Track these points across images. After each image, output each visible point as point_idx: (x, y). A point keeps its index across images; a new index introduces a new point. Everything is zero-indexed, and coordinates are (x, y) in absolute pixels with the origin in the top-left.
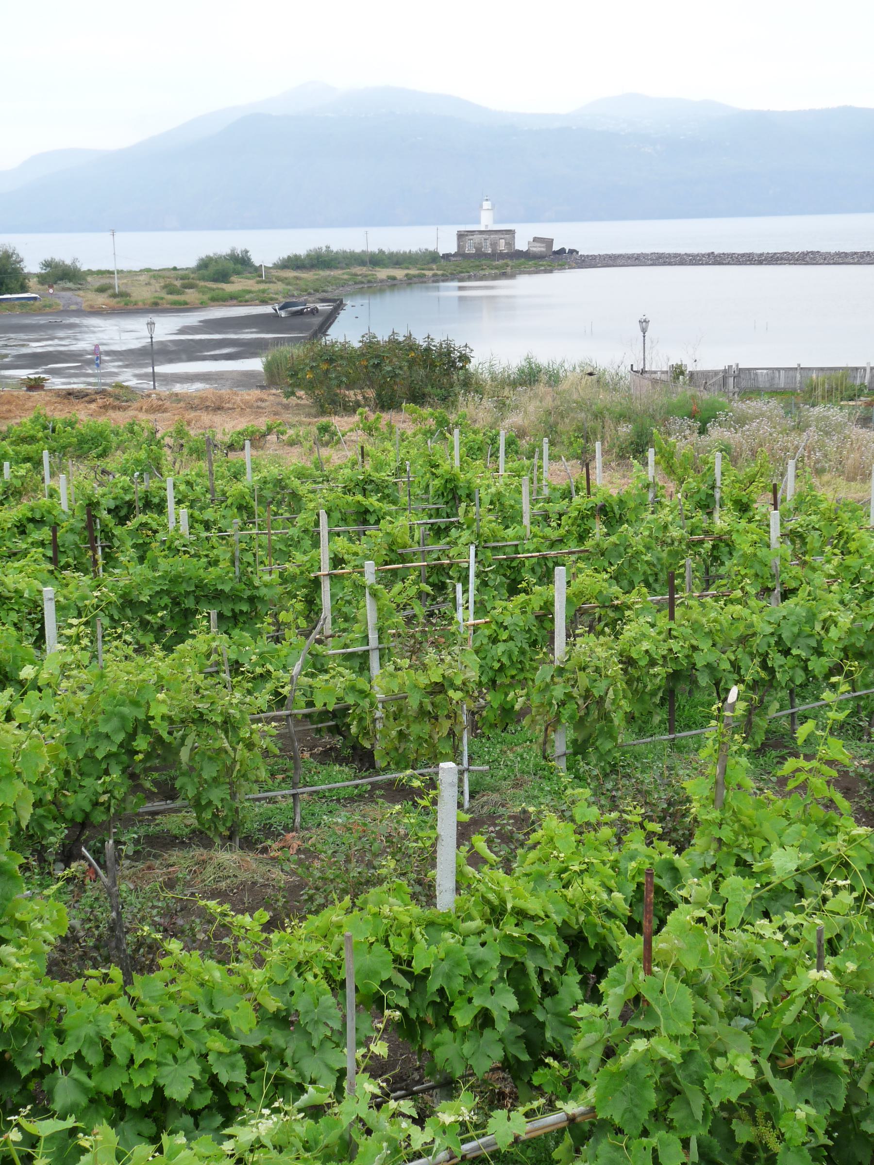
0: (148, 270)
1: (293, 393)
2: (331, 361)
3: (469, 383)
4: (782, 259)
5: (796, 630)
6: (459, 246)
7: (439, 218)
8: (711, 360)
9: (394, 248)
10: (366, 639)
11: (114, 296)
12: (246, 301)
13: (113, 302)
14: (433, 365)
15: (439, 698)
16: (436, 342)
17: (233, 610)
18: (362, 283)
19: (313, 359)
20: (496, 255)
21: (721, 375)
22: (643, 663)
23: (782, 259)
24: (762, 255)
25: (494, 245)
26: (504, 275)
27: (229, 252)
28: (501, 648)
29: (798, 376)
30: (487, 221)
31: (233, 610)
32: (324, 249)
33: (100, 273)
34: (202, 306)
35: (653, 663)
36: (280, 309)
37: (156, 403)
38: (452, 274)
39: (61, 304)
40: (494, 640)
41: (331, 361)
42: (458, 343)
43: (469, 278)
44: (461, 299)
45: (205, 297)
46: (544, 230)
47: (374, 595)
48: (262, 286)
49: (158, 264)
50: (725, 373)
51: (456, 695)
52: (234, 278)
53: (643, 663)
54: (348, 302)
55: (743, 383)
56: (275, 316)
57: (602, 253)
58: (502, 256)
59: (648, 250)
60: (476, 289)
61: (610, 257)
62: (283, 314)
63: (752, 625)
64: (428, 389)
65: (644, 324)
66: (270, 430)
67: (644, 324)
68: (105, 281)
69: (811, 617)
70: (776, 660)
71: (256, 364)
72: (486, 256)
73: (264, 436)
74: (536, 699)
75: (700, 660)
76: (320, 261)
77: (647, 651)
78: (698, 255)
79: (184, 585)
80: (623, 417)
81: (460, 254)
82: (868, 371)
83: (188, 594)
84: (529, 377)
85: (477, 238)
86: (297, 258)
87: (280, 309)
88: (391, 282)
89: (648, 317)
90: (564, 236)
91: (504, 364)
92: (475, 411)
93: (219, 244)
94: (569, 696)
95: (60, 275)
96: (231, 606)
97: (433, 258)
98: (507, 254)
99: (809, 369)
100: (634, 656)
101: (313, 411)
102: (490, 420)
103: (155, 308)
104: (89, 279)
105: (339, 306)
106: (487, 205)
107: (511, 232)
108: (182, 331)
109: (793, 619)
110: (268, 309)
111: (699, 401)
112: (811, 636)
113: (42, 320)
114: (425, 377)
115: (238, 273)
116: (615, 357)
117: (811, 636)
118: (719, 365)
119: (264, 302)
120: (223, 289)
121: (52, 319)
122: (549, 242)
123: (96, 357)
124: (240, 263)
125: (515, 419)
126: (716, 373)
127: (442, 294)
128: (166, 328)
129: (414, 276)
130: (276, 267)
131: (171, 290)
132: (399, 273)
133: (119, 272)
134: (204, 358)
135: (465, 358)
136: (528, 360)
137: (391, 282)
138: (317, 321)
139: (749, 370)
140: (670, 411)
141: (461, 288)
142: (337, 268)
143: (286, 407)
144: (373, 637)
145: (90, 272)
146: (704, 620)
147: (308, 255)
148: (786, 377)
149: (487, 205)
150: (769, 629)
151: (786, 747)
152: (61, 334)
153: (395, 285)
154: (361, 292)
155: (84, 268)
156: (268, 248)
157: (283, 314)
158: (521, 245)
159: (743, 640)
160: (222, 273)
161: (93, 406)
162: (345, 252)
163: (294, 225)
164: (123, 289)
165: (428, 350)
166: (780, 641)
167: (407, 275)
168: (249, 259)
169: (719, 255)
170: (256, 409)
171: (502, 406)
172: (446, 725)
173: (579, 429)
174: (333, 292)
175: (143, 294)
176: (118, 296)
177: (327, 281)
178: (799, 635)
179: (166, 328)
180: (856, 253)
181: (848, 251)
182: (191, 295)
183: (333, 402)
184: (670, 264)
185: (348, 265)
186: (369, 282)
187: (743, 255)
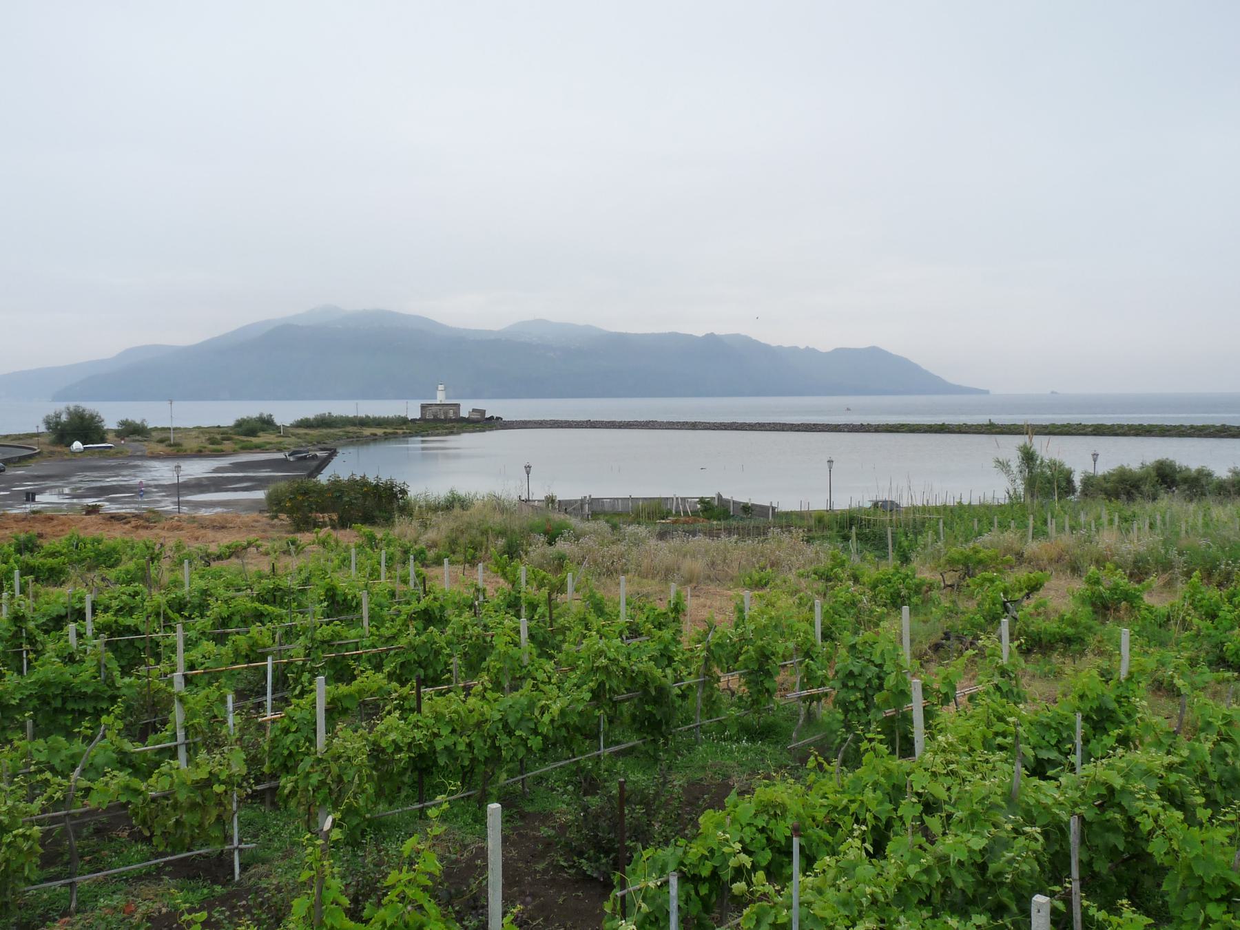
0: (199, 428)
1: (276, 517)
2: (305, 493)
3: (406, 510)
5: (519, 716)
8: (565, 493)
10: (174, 736)
11: (170, 445)
13: (169, 450)
14: (380, 497)
15: (207, 792)
16: (383, 480)
17: (95, 708)
19: (292, 493)
20: (447, 420)
22: (390, 751)
25: (446, 413)
26: (452, 433)
28: (291, 737)
30: (441, 398)
31: (95, 708)
33: (163, 429)
34: (235, 452)
35: (398, 749)
37: (175, 523)
39: (130, 451)
40: (286, 731)
41: (305, 493)
42: (399, 481)
43: (428, 435)
44: (423, 449)
45: (237, 447)
46: (480, 404)
47: (181, 700)
48: (281, 439)
49: (206, 423)
50: (583, 501)
51: (218, 789)
52: (260, 434)
53: (390, 751)
54: (340, 451)
55: (594, 509)
56: (286, 460)
58: (451, 421)
59: (548, 418)
60: (435, 442)
61: (524, 422)
62: (291, 459)
63: (482, 714)
64: (377, 513)
65: (528, 469)
66: (250, 544)
68: (164, 435)
69: (531, 705)
70: (503, 740)
71: (260, 495)
73: (245, 548)
74: (301, 785)
75: (439, 746)
76: (324, 422)
77: (394, 741)
79: (53, 689)
80: (502, 533)
81: (423, 419)
83: (55, 696)
84: (453, 504)
86: (307, 420)
90: (492, 408)
91: (435, 494)
92: (403, 529)
93: (251, 410)
94: (323, 783)
95: (131, 431)
96: (93, 704)
97: (404, 421)
100: (383, 745)
101: (292, 529)
102: (415, 535)
103: (199, 454)
104: (154, 434)
105: (333, 453)
106: (441, 387)
107: (458, 405)
108: (215, 471)
109: (517, 707)
110: (281, 456)
111: (551, 522)
112: (530, 720)
113: (113, 463)
114: (379, 503)
115: (263, 430)
116: (510, 489)
117: (530, 720)
118: (577, 496)
119: (280, 450)
121: (121, 462)
122: (483, 412)
123: (140, 491)
124: (266, 424)
125: (431, 535)
126: (576, 501)
128: (197, 469)
130: (292, 426)
131: (213, 441)
132: (379, 431)
133: (175, 429)
134: (235, 490)
135: (404, 492)
136: (452, 492)
138: (315, 463)
140: (532, 530)
143: (273, 526)
144: (181, 734)
145: (156, 429)
146: (446, 711)
147: (315, 419)
149: (441, 387)
150: (498, 716)
151: (516, 807)
152: (124, 473)
154: (352, 444)
155: (150, 426)
156: (286, 413)
157: (291, 459)
158: (464, 413)
159: (479, 725)
160: (252, 430)
161: (127, 526)
163: (708, 396)
164: (178, 441)
165: (377, 486)
166: (506, 725)
170: (249, 528)
171: (425, 525)
172: (214, 813)
173: (471, 542)
174: (330, 444)
175: (191, 444)
176: (173, 445)
177: (328, 436)
178: (521, 719)
179: (197, 469)
182: (227, 446)
183: (307, 523)
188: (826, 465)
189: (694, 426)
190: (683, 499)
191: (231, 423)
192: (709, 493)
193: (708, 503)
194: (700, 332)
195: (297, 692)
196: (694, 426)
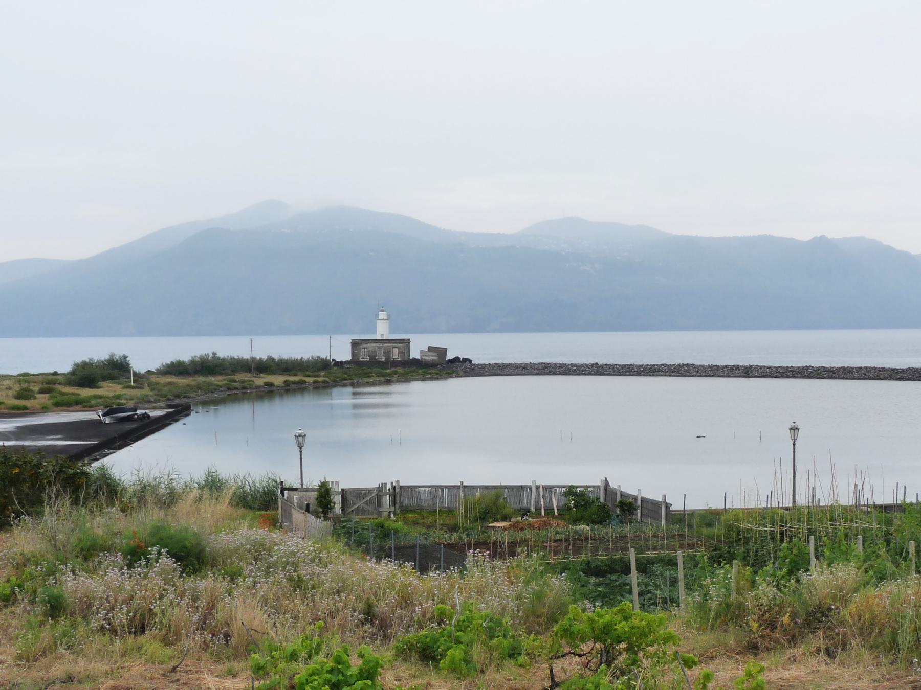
4: (659, 370)
6: (353, 354)
7: (337, 330)
9: (286, 356)
12: (91, 407)
18: (236, 389)
21: (375, 493)
23: (659, 370)
24: (641, 366)
25: (388, 353)
27: (107, 357)
29: (462, 495)
30: (382, 331)
32: (211, 355)
34: (44, 410)
36: (104, 415)
38: (334, 381)
44: (356, 407)
46: (438, 341)
52: (104, 384)
57: (492, 362)
58: (395, 364)
60: (374, 395)
62: (108, 420)
65: (794, 429)
67: (794, 429)
72: (379, 363)
78: (582, 366)
81: (355, 362)
82: (534, 489)
85: (371, 346)
87: (104, 415)
88: (268, 388)
89: (799, 425)
93: (98, 350)
97: (323, 365)
98: (400, 362)
99: (473, 487)
106: (382, 315)
120: (78, 395)
122: (442, 352)
124: (117, 369)
126: (370, 491)
127: (335, 402)
129: (294, 383)
132: (278, 380)
136: (210, 474)
137: (268, 388)
139: (411, 487)
141: (355, 394)
142: (221, 374)
147: (193, 362)
148: (450, 496)
153: (272, 391)
157: (108, 420)
158: (415, 354)
162: (233, 359)
167: (286, 381)
168: (128, 365)
169: (602, 366)
180: (726, 366)
181: (719, 364)
184: (555, 374)
185: (234, 372)
186: (244, 388)
187: (623, 366)
188: (787, 434)
189: (747, 372)
190: (548, 489)
191: (65, 368)
192: (585, 475)
193: (582, 494)
194: (804, 233)
195: (649, 595)
196: (747, 372)
